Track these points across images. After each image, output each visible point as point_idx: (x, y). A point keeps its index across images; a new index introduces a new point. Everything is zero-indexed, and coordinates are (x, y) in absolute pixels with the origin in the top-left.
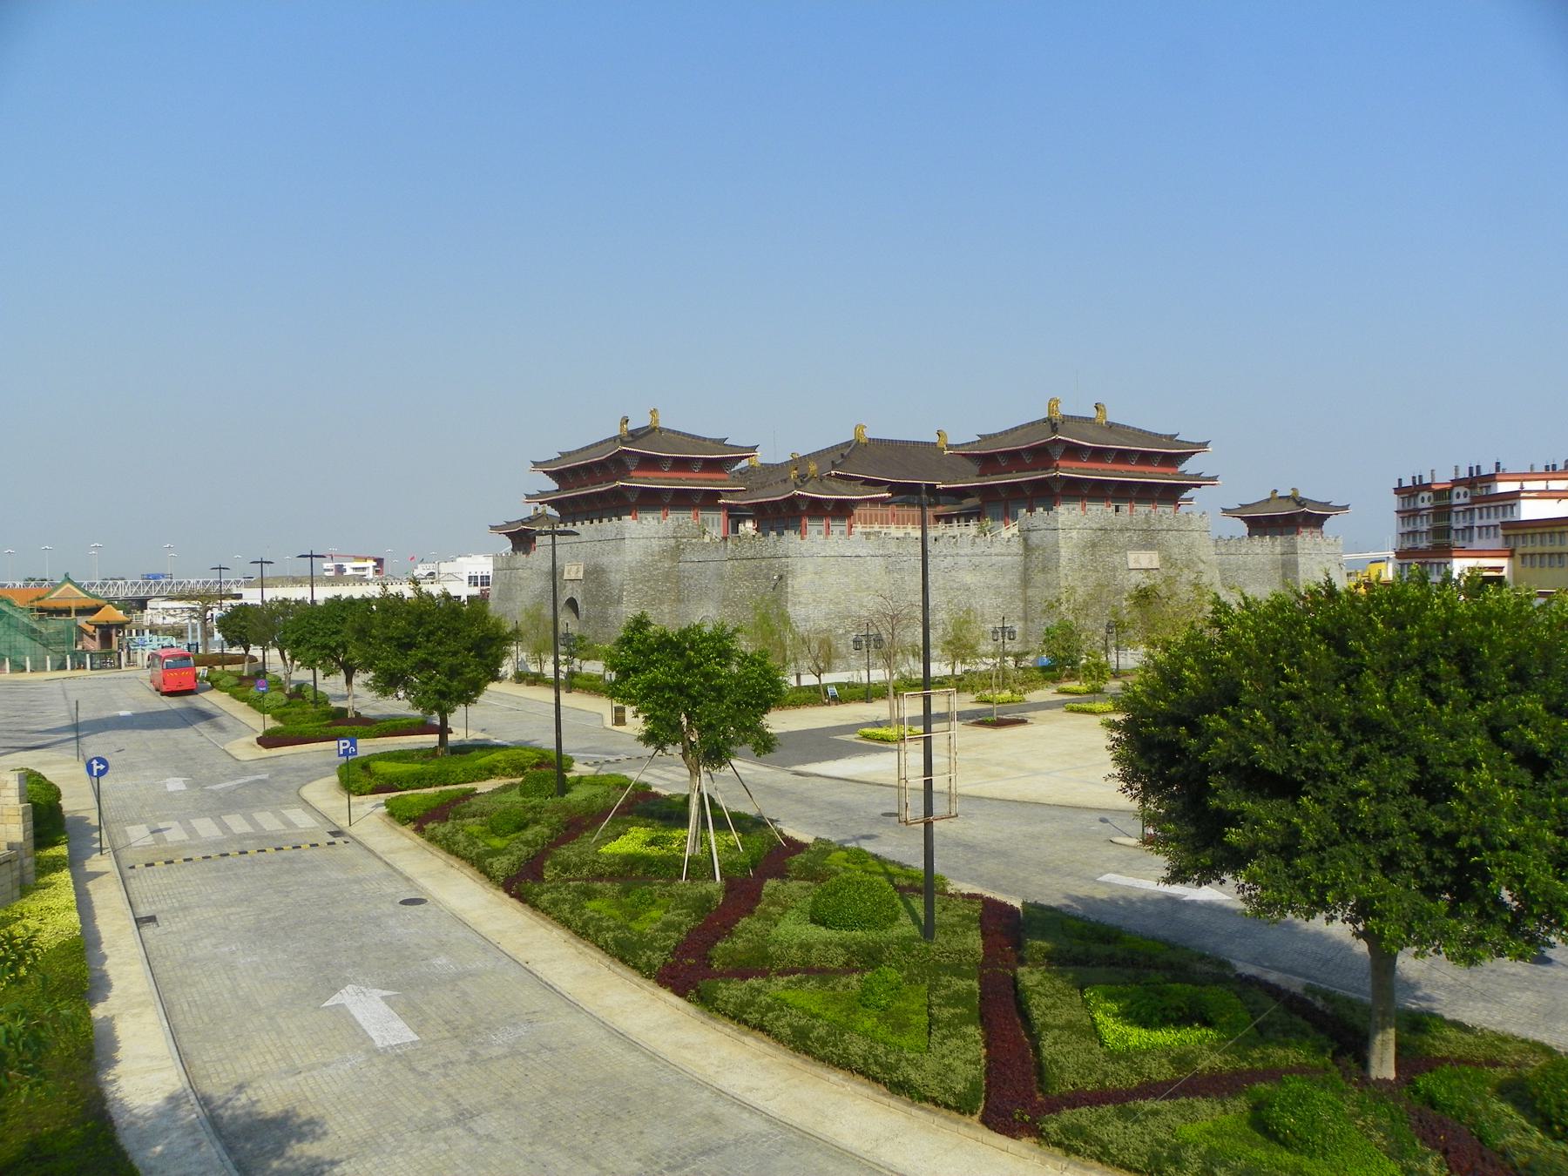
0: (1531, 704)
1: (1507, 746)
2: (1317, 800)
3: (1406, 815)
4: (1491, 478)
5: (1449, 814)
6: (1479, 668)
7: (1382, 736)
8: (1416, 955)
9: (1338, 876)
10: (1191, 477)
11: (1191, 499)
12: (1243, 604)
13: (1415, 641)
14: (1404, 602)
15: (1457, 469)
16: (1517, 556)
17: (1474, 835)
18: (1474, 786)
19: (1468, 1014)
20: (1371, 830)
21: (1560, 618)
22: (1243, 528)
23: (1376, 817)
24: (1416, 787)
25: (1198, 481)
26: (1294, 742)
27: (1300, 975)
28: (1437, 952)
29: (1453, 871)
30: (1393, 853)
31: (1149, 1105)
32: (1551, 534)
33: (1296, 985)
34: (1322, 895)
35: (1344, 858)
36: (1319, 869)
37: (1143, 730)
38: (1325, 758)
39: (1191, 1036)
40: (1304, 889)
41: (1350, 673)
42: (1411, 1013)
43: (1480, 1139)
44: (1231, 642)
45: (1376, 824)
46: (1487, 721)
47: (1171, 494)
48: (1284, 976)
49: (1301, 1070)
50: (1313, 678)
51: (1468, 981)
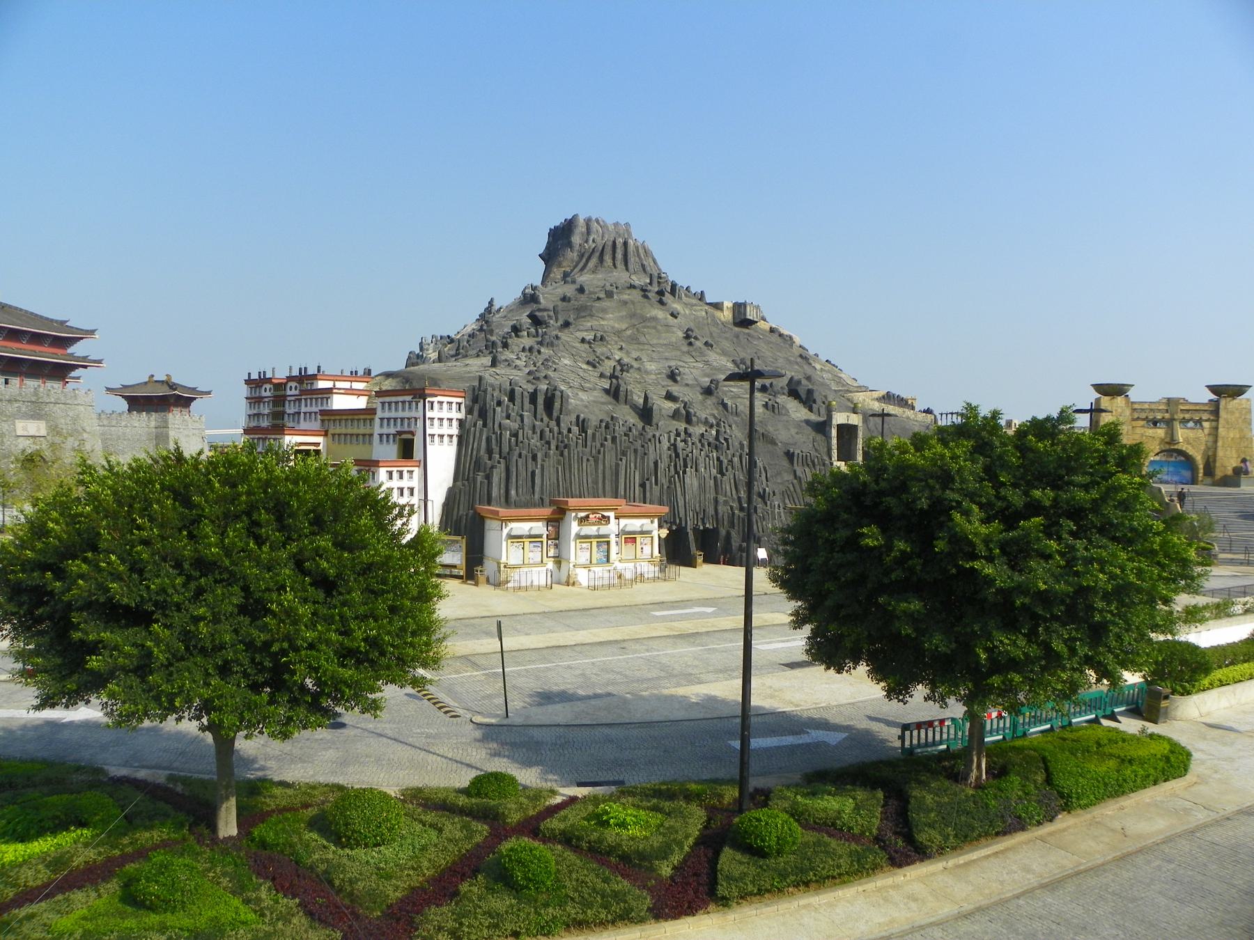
0: (324, 542)
1: (304, 572)
2: (165, 626)
3: (236, 631)
4: (314, 377)
5: (264, 628)
6: (289, 516)
7: (217, 572)
8: (246, 737)
9: (183, 685)
10: (78, 359)
11: (78, 378)
12: (107, 467)
13: (244, 498)
14: (235, 466)
15: (291, 368)
16: (330, 435)
17: (283, 641)
18: (282, 605)
19: (290, 775)
20: (209, 645)
21: (345, 480)
22: (124, 405)
23: (212, 635)
24: (243, 610)
25: (84, 363)
26: (145, 580)
27: (165, 768)
28: (261, 733)
29: (270, 670)
30: (226, 662)
31: (23, 912)
32: (352, 420)
33: (160, 777)
34: (171, 702)
35: (188, 670)
36: (168, 681)
37: (11, 577)
38: (170, 591)
39: (66, 839)
40: (157, 698)
41: (193, 522)
42: (249, 781)
43: (297, 863)
44: (92, 498)
45: (213, 641)
46: (294, 555)
47: (60, 372)
48: (148, 771)
49: (165, 844)
50: (162, 526)
51: (291, 750)
